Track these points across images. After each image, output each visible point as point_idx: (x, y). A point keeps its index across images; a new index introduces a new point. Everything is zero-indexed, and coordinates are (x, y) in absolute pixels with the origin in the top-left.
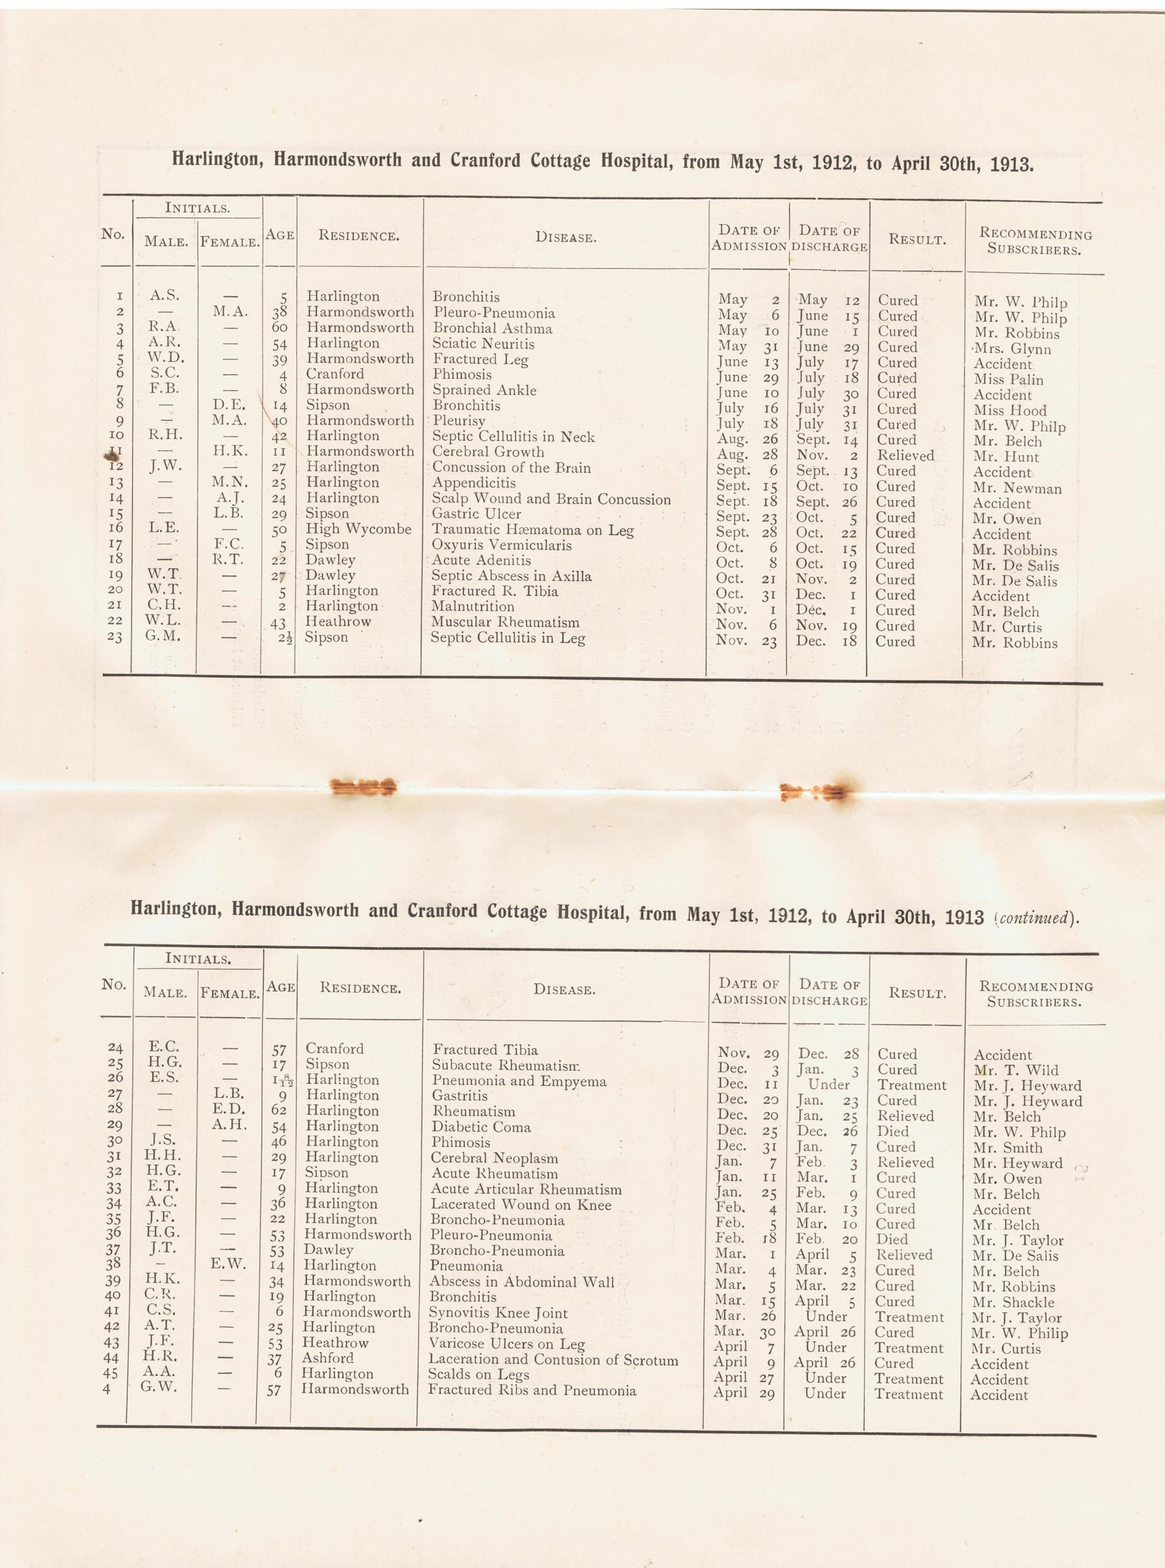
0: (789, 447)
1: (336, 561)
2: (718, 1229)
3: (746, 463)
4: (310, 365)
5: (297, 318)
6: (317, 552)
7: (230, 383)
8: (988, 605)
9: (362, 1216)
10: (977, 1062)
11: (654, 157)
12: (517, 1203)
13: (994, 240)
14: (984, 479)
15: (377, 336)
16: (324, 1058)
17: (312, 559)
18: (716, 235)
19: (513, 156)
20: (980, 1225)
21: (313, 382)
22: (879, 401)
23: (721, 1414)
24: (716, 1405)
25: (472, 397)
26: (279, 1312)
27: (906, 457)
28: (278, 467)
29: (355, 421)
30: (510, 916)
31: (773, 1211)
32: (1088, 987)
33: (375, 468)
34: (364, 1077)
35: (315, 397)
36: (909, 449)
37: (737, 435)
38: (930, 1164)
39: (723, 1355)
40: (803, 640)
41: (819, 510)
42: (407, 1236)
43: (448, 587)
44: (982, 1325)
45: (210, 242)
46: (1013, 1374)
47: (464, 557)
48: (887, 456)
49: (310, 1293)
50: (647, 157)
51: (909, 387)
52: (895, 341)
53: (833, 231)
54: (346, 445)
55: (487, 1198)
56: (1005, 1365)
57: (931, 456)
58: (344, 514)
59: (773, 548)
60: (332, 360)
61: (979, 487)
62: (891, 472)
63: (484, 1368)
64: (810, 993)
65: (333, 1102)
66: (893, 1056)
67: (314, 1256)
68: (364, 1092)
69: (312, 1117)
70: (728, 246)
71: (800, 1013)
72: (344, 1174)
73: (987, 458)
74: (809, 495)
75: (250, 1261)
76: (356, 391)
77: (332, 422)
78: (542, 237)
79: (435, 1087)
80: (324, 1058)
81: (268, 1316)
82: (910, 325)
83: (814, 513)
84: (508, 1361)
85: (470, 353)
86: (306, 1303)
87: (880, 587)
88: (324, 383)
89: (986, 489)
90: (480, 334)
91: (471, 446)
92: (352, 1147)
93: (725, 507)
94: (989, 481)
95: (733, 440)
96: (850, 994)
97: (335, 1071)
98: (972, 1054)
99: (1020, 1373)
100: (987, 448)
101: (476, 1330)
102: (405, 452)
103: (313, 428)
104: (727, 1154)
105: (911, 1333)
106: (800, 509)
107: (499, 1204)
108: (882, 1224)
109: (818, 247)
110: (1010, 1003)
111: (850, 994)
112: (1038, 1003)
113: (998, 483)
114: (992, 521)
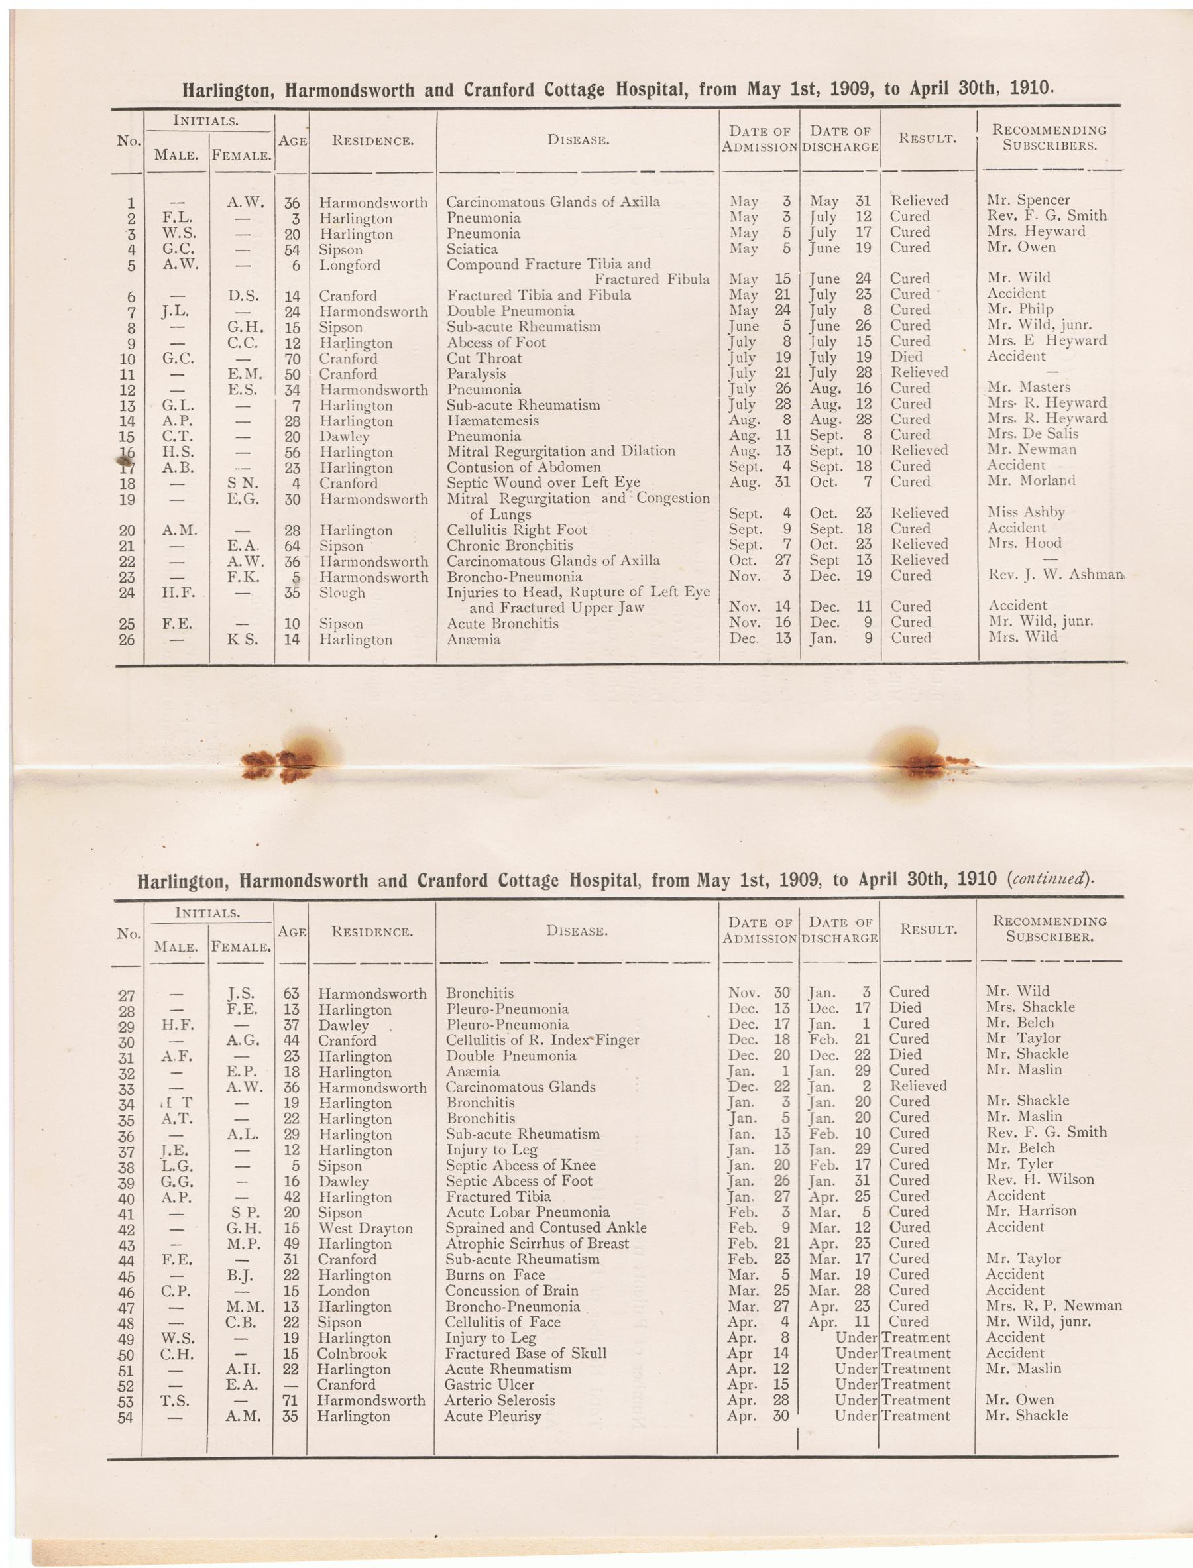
1: (350, 438)
2: (731, 1251)
3: (758, 460)
4: (322, 1251)
5: (310, 1006)
6: (330, 1174)
7: (244, 461)
8: (1004, 302)
9: (376, 1116)
10: (988, 1360)
11: (669, 85)
13: (1008, 137)
14: (1000, 612)
16: (337, 305)
17: (325, 1181)
18: (726, 136)
19: (527, 85)
20: (996, 308)
22: (891, 1204)
24: (730, 1430)
25: (486, 1094)
26: (296, 1166)
27: (920, 452)
28: (292, 234)
29: (369, 563)
30: (521, 885)
32: (1102, 130)
33: (388, 407)
34: (376, 1335)
35: (328, 585)
36: (922, 444)
37: (749, 416)
38: (944, 1086)
41: (833, 537)
42: (424, 313)
43: (462, 1350)
44: (998, 1156)
45: (221, 155)
46: (1028, 1346)
47: (477, 1366)
48: (901, 560)
49: (326, 465)
50: (662, 85)
51: (921, 1142)
52: (907, 1142)
55: (502, 1191)
56: (1021, 1338)
57: (944, 1086)
58: (358, 1214)
59: (787, 326)
60: (346, 563)
61: (993, 1211)
62: (906, 390)
63: (497, 1269)
64: (820, 931)
65: (345, 1063)
66: (906, 608)
67: (330, 1188)
68: (376, 1132)
69: (325, 1080)
70: (739, 148)
71: (812, 159)
72: (357, 1324)
73: (1000, 1213)
74: (822, 554)
75: (265, 1082)
76: (369, 313)
77: (343, 1402)
78: (553, 930)
79: (450, 1032)
80: (337, 305)
81: (285, 1164)
82: (921, 1127)
83: (828, 541)
85: (482, 1190)
86: (322, 1095)
87: (894, 1109)
89: (1001, 279)
90: (491, 1032)
91: (483, 1222)
92: (366, 1141)
94: (1003, 1205)
95: (744, 421)
96: (861, 140)
97: (346, 1329)
98: (986, 604)
99: (1037, 1346)
100: (999, 1061)
101: (493, 1308)
102: (419, 204)
103: (326, 459)
104: (739, 1064)
105: (927, 529)
106: (813, 536)
107: (515, 1197)
108: (896, 1039)
109: (828, 147)
110: (1027, 146)
111: (861, 140)
112: (1055, 146)
113: (1012, 1207)
114: (1004, 1417)
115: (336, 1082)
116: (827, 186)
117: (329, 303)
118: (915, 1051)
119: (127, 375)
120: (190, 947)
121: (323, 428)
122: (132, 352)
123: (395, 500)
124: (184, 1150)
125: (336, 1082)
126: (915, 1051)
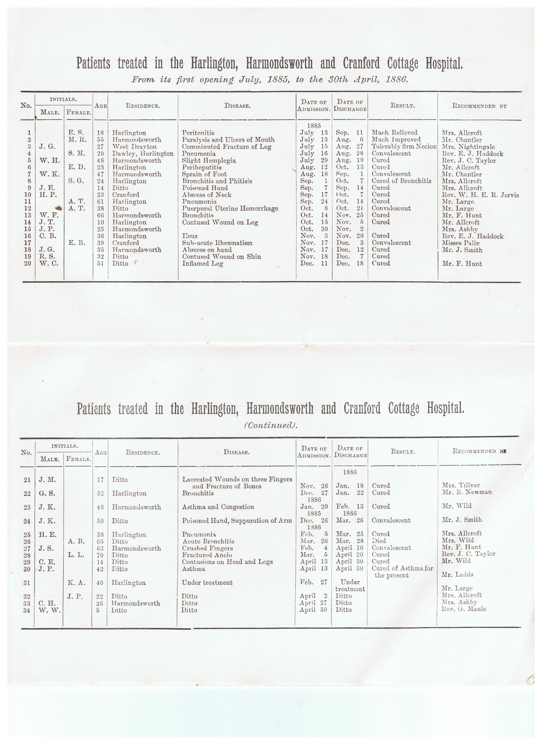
0: (332, 170)
5: (108, 139)
12: (219, 256)
15: (144, 164)
21: (115, 247)
23: (304, 620)
31: (326, 548)
39: (304, 565)
40: (339, 263)
53: (352, 449)
54: (130, 226)
84: (217, 182)
88: (120, 247)
93: (304, 184)
115: (120, 172)
116: (342, 126)
117: (117, 246)
118: (383, 539)
119: (28, 202)
120: (56, 459)
121: (113, 538)
122: (29, 191)
123: (146, 549)
124: (53, 188)
125: (120, 172)
126: (383, 539)
